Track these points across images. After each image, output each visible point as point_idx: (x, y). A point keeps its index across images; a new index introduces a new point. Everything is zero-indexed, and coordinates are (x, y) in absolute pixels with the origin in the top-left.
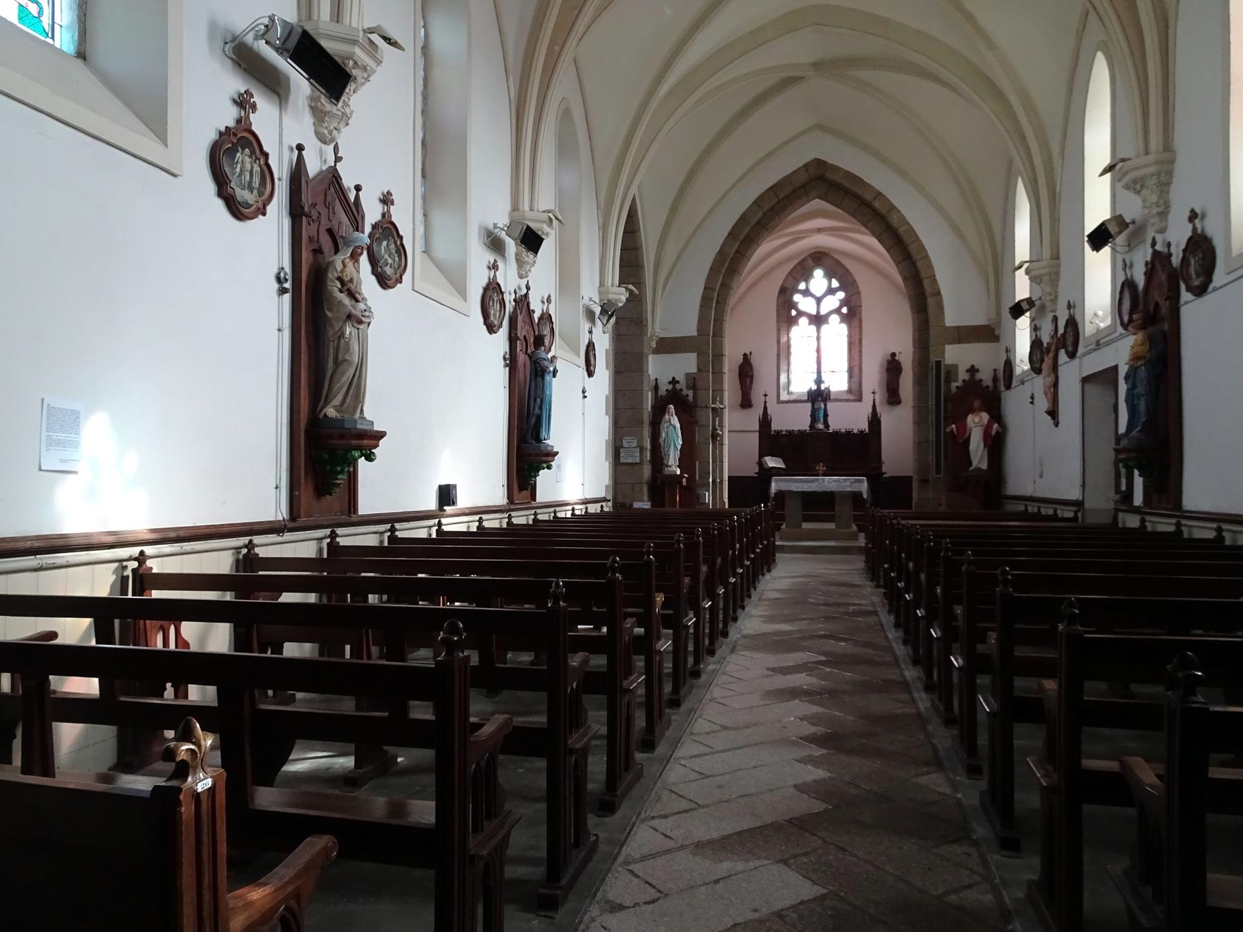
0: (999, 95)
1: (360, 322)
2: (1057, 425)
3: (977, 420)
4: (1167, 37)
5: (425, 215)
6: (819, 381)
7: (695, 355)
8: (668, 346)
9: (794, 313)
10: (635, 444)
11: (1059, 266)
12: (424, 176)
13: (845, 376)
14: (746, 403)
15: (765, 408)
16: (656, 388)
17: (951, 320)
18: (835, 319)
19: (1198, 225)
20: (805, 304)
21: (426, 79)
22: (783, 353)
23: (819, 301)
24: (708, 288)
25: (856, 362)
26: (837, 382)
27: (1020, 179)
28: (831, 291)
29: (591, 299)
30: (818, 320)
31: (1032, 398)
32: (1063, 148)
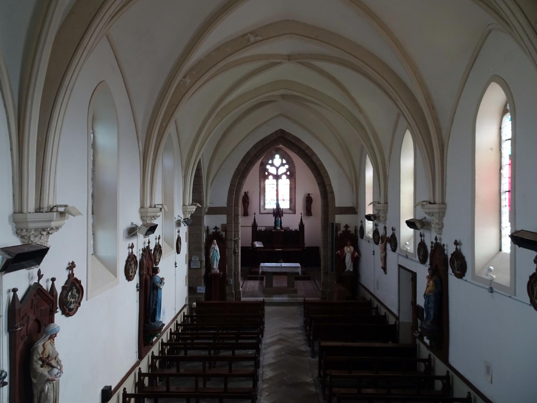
0: (363, 129)
1: (53, 380)
2: (386, 273)
3: (349, 249)
4: (443, 154)
5: (93, 234)
6: (278, 205)
7: (226, 215)
8: (213, 211)
9: (266, 173)
10: (198, 259)
11: (387, 207)
12: (93, 214)
13: (288, 202)
14: (246, 214)
15: (255, 220)
16: (208, 230)
17: (337, 205)
18: (284, 177)
19: (458, 247)
20: (272, 170)
21: (94, 161)
22: (262, 191)
23: (277, 168)
24: (232, 185)
25: (293, 197)
26: (285, 205)
27: (367, 156)
28: (283, 165)
29: (179, 216)
30: (277, 177)
31: (374, 252)
32: (390, 157)
